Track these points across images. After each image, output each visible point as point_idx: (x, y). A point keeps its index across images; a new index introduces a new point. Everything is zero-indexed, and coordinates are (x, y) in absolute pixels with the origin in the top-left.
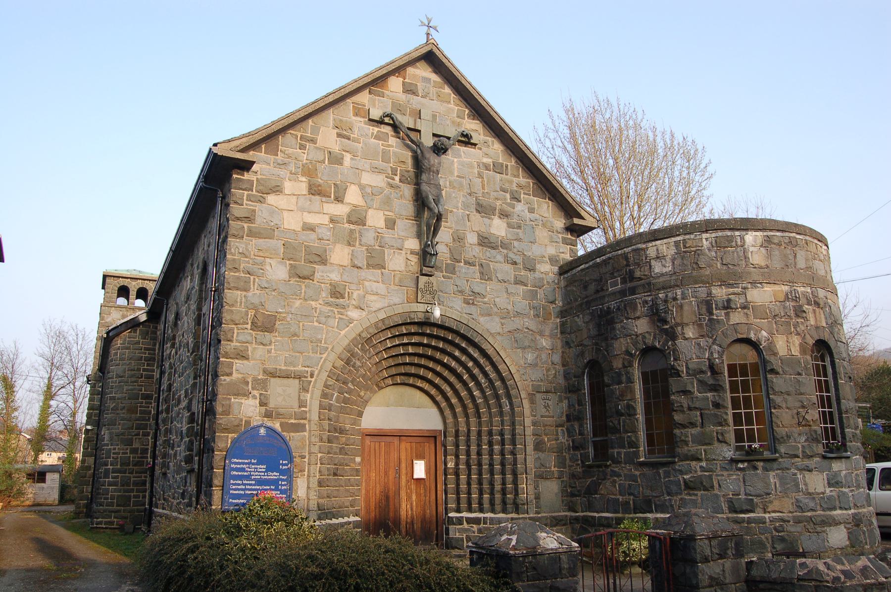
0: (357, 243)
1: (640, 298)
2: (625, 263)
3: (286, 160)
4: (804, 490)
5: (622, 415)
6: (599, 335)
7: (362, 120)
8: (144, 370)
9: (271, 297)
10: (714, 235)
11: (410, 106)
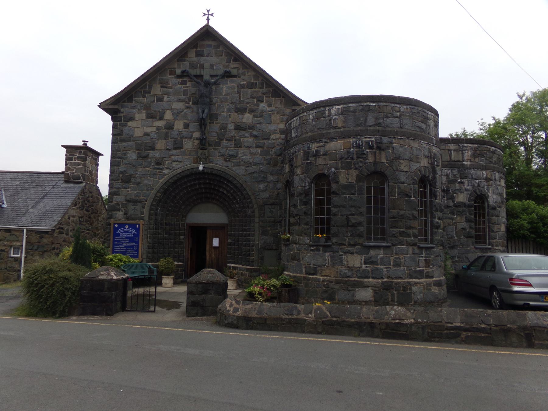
3: (136, 105)
4: (346, 265)
9: (129, 168)
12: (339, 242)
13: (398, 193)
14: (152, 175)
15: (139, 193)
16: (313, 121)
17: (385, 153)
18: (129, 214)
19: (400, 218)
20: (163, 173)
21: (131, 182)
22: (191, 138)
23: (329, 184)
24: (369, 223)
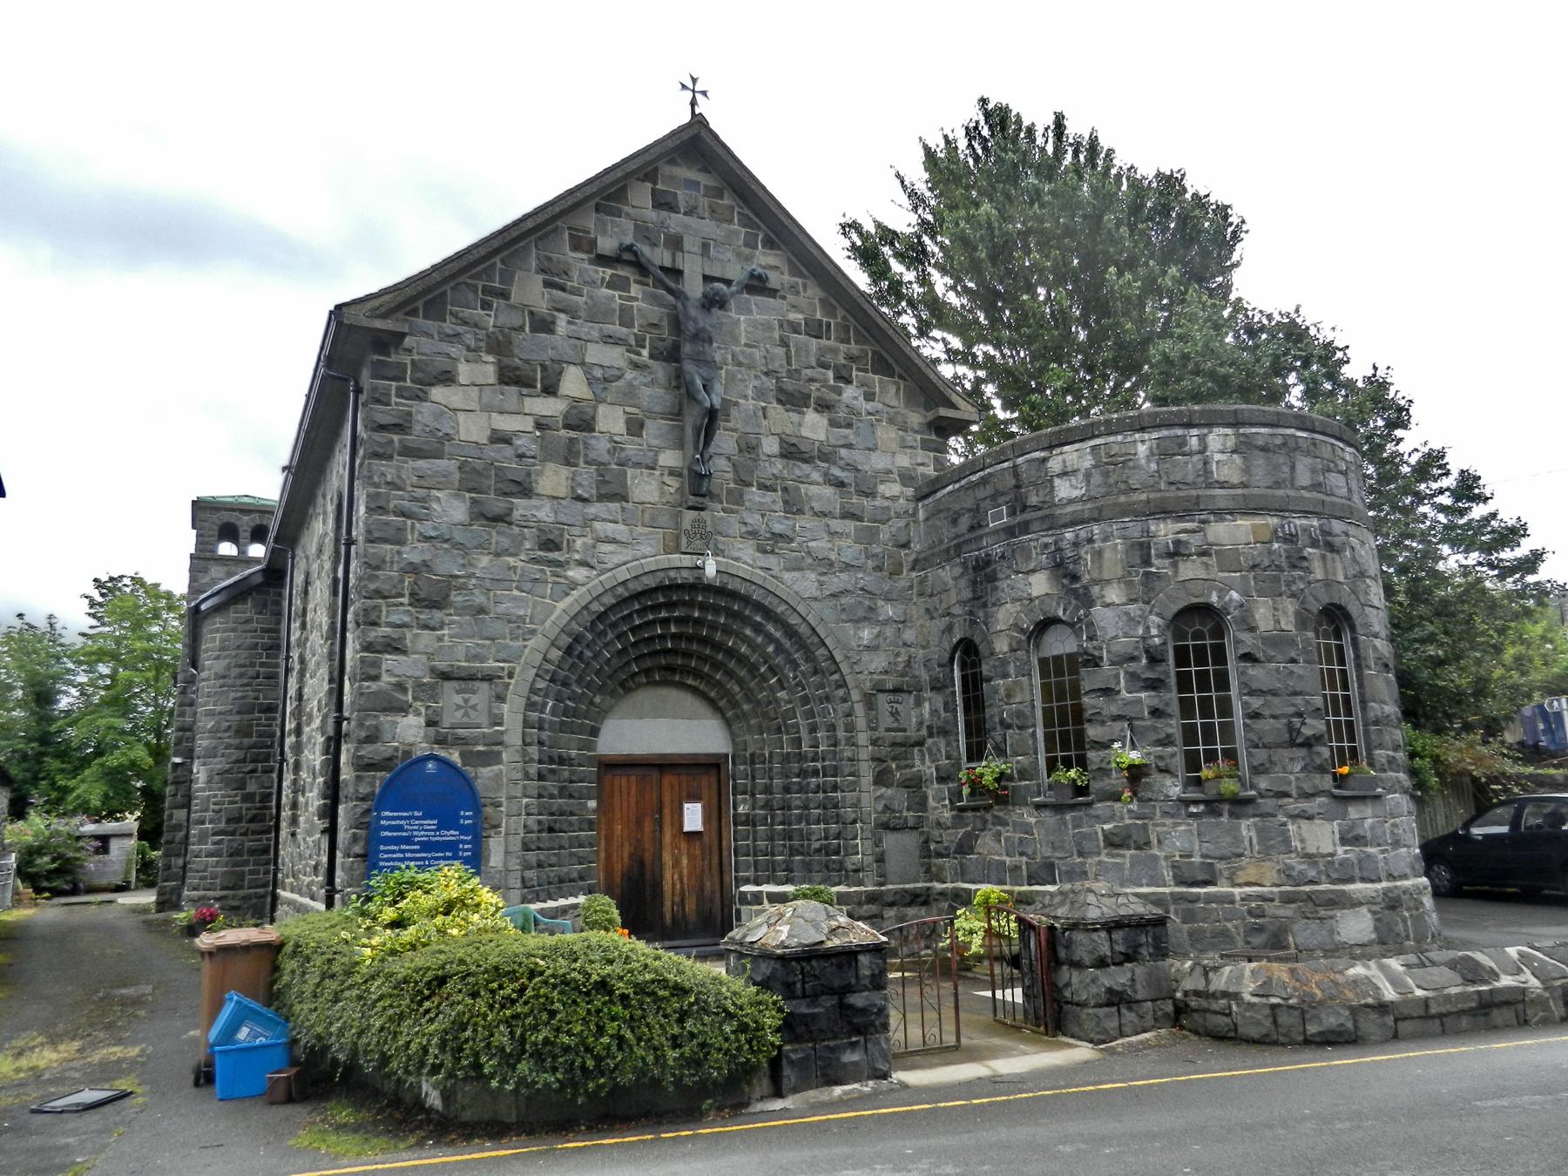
0: (582, 460)
1: (1036, 540)
2: (1013, 482)
5: (1009, 727)
6: (974, 599)
7: (584, 256)
8: (262, 665)
10: (1155, 435)
12: (1276, 789)
14: (529, 585)
15: (484, 646)
16: (1149, 461)
18: (446, 723)
20: (566, 578)
21: (451, 605)
22: (654, 469)
23: (1219, 631)
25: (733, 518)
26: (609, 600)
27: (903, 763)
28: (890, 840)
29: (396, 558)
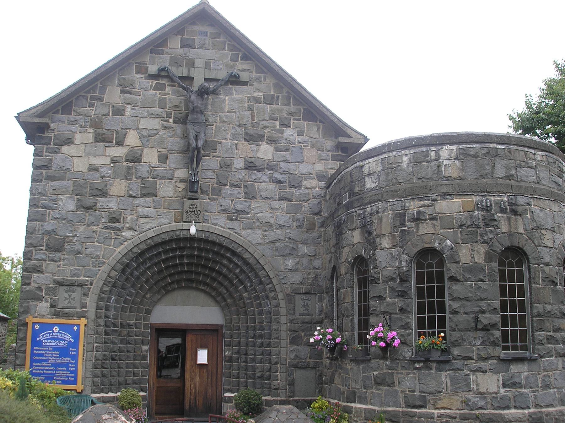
3: (77, 118)
4: (475, 390)
7: (142, 76)
11: (187, 58)
13: (542, 279)
14: (103, 240)
16: (408, 166)
17: (522, 219)
18: (60, 306)
19: (546, 315)
20: (122, 236)
22: (172, 179)
23: (441, 263)
24: (505, 324)
25: (214, 203)
26: (143, 247)
27: (308, 333)
28: (298, 374)
29: (41, 228)
